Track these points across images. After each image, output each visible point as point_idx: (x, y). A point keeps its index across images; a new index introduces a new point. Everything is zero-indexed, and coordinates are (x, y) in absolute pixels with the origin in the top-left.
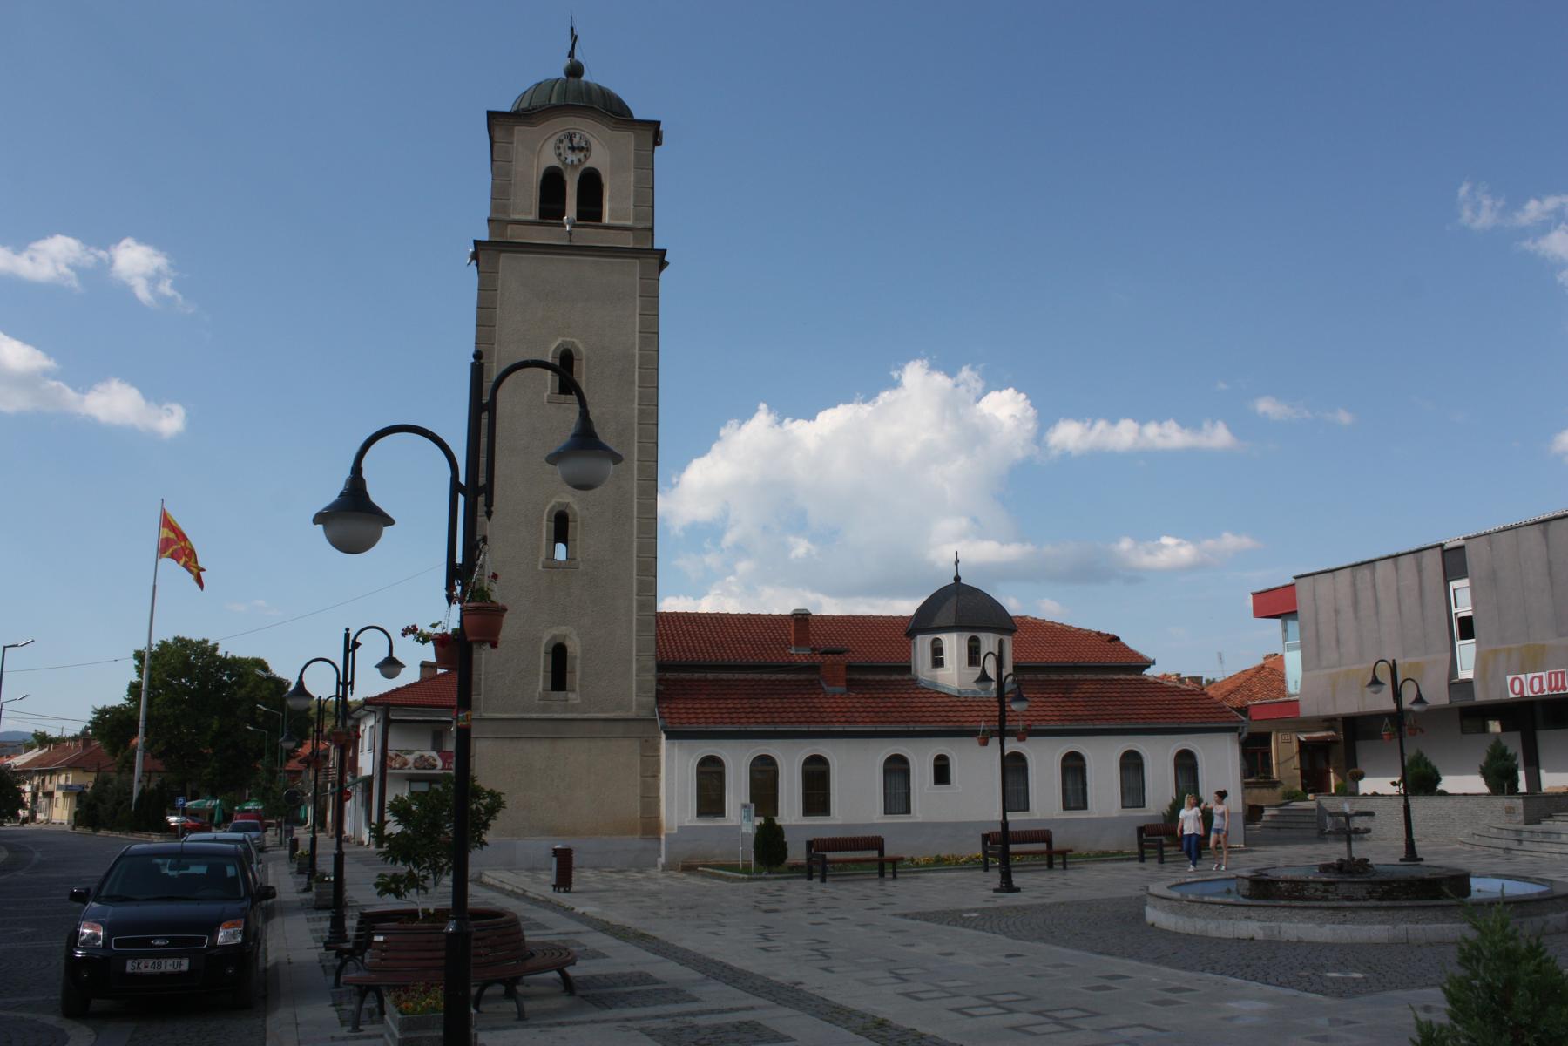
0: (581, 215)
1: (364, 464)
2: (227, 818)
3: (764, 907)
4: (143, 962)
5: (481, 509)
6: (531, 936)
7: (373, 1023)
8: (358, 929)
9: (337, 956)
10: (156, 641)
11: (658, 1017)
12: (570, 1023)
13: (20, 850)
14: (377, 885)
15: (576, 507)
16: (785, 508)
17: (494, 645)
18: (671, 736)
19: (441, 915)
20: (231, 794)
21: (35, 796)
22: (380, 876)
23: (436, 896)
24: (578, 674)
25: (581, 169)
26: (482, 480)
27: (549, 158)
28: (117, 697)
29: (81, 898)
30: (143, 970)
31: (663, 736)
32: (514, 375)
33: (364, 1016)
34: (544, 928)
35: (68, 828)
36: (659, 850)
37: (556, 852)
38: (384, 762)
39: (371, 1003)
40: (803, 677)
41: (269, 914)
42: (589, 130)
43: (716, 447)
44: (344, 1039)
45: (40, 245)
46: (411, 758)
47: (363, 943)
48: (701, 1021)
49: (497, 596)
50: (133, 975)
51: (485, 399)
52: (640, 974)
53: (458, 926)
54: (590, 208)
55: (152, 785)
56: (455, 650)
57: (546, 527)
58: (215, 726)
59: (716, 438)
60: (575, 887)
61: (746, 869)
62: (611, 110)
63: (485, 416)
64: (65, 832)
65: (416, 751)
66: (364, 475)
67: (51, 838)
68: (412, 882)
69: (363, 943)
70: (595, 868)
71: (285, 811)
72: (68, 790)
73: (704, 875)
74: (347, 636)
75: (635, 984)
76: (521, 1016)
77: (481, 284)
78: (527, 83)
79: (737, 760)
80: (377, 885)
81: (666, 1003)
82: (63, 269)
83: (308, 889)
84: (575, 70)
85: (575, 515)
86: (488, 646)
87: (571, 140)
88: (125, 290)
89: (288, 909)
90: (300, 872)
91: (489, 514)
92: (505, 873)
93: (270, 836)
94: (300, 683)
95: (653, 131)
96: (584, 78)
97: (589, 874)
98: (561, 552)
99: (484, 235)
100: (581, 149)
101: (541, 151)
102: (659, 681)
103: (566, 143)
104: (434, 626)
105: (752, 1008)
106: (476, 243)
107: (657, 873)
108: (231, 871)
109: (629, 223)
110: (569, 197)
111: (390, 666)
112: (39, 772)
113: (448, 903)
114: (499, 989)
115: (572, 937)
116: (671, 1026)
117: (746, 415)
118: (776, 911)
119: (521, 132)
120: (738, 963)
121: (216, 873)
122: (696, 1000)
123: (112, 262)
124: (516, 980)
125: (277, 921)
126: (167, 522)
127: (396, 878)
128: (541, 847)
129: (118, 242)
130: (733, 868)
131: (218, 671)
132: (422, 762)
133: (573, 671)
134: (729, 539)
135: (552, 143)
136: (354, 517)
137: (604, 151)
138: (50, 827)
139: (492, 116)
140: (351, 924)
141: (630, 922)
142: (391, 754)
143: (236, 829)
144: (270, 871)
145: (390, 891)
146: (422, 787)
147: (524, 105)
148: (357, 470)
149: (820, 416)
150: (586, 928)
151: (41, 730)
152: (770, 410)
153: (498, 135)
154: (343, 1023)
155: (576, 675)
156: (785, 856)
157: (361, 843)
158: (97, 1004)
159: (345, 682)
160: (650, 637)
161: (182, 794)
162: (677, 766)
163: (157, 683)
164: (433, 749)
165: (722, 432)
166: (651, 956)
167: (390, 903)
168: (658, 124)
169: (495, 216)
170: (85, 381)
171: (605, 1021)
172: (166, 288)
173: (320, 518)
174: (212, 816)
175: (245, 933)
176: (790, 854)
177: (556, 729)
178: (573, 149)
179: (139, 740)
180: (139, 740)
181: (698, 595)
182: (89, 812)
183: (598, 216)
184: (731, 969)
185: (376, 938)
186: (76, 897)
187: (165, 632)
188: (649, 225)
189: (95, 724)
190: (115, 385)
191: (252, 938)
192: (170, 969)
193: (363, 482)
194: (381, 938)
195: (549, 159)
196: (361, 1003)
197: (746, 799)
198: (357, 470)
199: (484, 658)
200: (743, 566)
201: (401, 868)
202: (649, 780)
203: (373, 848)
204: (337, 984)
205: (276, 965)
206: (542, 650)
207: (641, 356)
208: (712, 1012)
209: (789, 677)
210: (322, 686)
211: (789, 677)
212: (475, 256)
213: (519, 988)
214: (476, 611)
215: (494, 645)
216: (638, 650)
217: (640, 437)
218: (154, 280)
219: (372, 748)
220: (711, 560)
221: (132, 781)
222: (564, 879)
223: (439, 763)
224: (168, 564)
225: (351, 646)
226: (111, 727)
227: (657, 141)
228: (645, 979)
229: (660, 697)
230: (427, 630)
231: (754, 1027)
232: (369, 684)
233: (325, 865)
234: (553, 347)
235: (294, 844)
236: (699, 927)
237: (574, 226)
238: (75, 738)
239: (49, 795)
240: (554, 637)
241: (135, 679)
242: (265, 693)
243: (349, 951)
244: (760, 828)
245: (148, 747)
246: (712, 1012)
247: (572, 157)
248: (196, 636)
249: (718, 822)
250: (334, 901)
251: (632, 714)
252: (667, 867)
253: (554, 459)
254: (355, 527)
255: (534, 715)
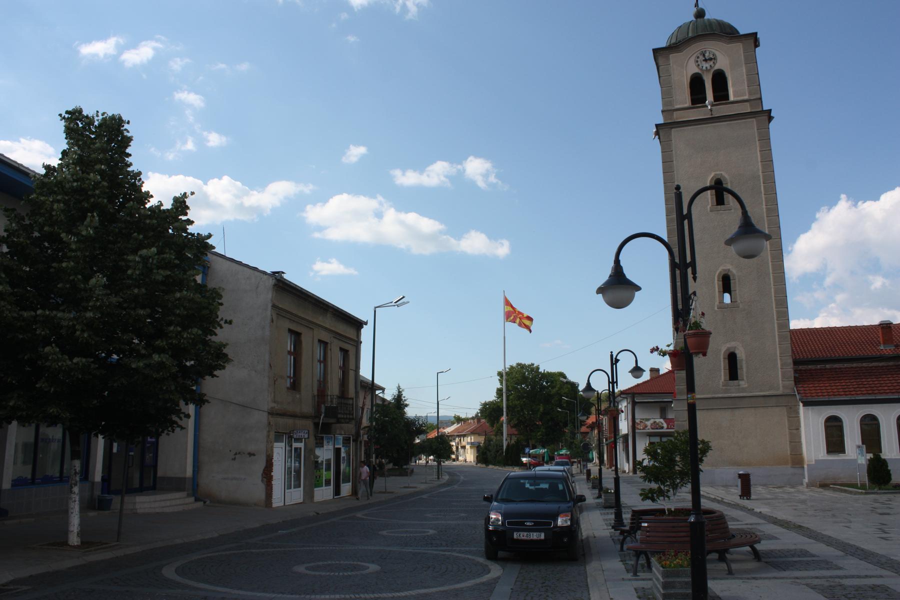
0: (716, 98)
1: (620, 258)
3: (879, 511)
4: (522, 533)
5: (690, 276)
6: (732, 525)
7: (644, 572)
8: (632, 519)
9: (621, 534)
10: (508, 366)
11: (817, 578)
12: (761, 578)
13: (454, 473)
15: (734, 271)
16: (865, 259)
17: (705, 354)
18: (806, 404)
19: (685, 512)
20: (552, 446)
21: (457, 448)
22: (642, 490)
24: (745, 370)
26: (689, 260)
27: (692, 69)
28: (492, 397)
29: (489, 499)
31: (801, 404)
32: (701, 195)
33: (639, 568)
35: (474, 464)
36: (803, 475)
37: (740, 476)
38: (634, 426)
40: (891, 363)
41: (581, 511)
42: (712, 47)
43: (814, 226)
44: (630, 580)
45: (430, 168)
46: (649, 423)
47: (635, 526)
48: (847, 582)
50: (517, 540)
51: (685, 212)
52: (801, 550)
53: (696, 518)
54: (721, 92)
55: (513, 442)
56: (682, 357)
57: (717, 285)
59: (814, 219)
60: (753, 497)
61: (863, 486)
62: (725, 32)
63: (686, 222)
64: (473, 466)
65: (651, 419)
66: (622, 264)
67: (465, 469)
68: (661, 493)
69: (635, 526)
70: (764, 485)
71: (581, 454)
72: (472, 444)
73: (834, 490)
74: (612, 356)
75: (799, 556)
76: (730, 572)
77: (662, 149)
78: (673, 28)
79: (851, 419)
80: (641, 495)
82: (443, 178)
83: (599, 497)
84: (700, 14)
85: (734, 275)
86: (701, 355)
87: (704, 56)
88: (472, 184)
89: (590, 508)
90: (594, 487)
91: (695, 278)
92: (717, 489)
93: (575, 469)
94: (589, 384)
97: (760, 488)
98: (727, 298)
100: (711, 59)
101: (687, 65)
102: (795, 371)
103: (701, 58)
104: (668, 346)
105: (881, 576)
106: (657, 126)
107: (803, 488)
108: (561, 487)
109: (746, 97)
110: (709, 89)
111: (637, 371)
112: (459, 436)
113: (689, 505)
116: (827, 584)
117: (832, 203)
118: (888, 514)
119: (673, 57)
121: (553, 488)
122: (840, 568)
123: (464, 170)
124: (726, 551)
126: (507, 303)
127: (651, 491)
128: (731, 473)
129: (466, 159)
131: (540, 380)
132: (655, 425)
133: (742, 368)
134: (828, 281)
135: (692, 60)
136: (618, 288)
137: (725, 57)
139: (656, 52)
140: (627, 517)
141: (789, 518)
142: (637, 421)
143: (557, 464)
146: (656, 440)
147: (673, 41)
148: (617, 261)
149: (883, 197)
150: (762, 521)
151: (458, 414)
152: (848, 199)
153: (661, 62)
154: (628, 571)
155: (743, 369)
156: (890, 479)
157: (624, 472)
158: (501, 554)
159: (613, 382)
160: (787, 345)
161: (528, 446)
162: (811, 424)
163: (510, 388)
165: (818, 216)
167: (648, 505)
168: (756, 34)
170: (459, 237)
172: (492, 179)
173: (600, 290)
174: (543, 458)
175: (571, 520)
176: (893, 477)
177: (733, 403)
178: (706, 60)
179: (504, 418)
180: (504, 418)
181: (812, 317)
182: (484, 455)
183: (726, 97)
184: (862, 550)
187: (512, 362)
188: (758, 96)
189: (482, 411)
190: (473, 233)
191: (575, 522)
192: (535, 538)
193: (621, 268)
194: (646, 525)
195: (693, 69)
196: (638, 560)
198: (617, 261)
200: (840, 297)
201: (654, 486)
202: (795, 431)
203: (631, 474)
205: (588, 538)
206: (722, 357)
207: (764, 176)
208: (853, 577)
209: (881, 364)
210: (601, 385)
211: (881, 364)
212: (657, 133)
213: (728, 556)
215: (705, 354)
218: (486, 176)
219: (627, 418)
220: (819, 295)
221: (502, 440)
222: (746, 492)
223: (665, 425)
224: (509, 325)
225: (614, 362)
226: (490, 412)
227: (756, 44)
228: (805, 553)
229: (797, 381)
230: (665, 348)
231: (885, 589)
232: (626, 382)
233: (608, 483)
235: (589, 472)
237: (712, 105)
238: (473, 418)
239: (464, 447)
240: (728, 349)
241: (499, 386)
242: (566, 390)
244: (870, 460)
246: (853, 577)
247: (706, 65)
248: (527, 362)
249: (841, 457)
250: (616, 504)
251: (780, 392)
252: (810, 485)
253: (729, 242)
254: (620, 294)
255: (720, 395)
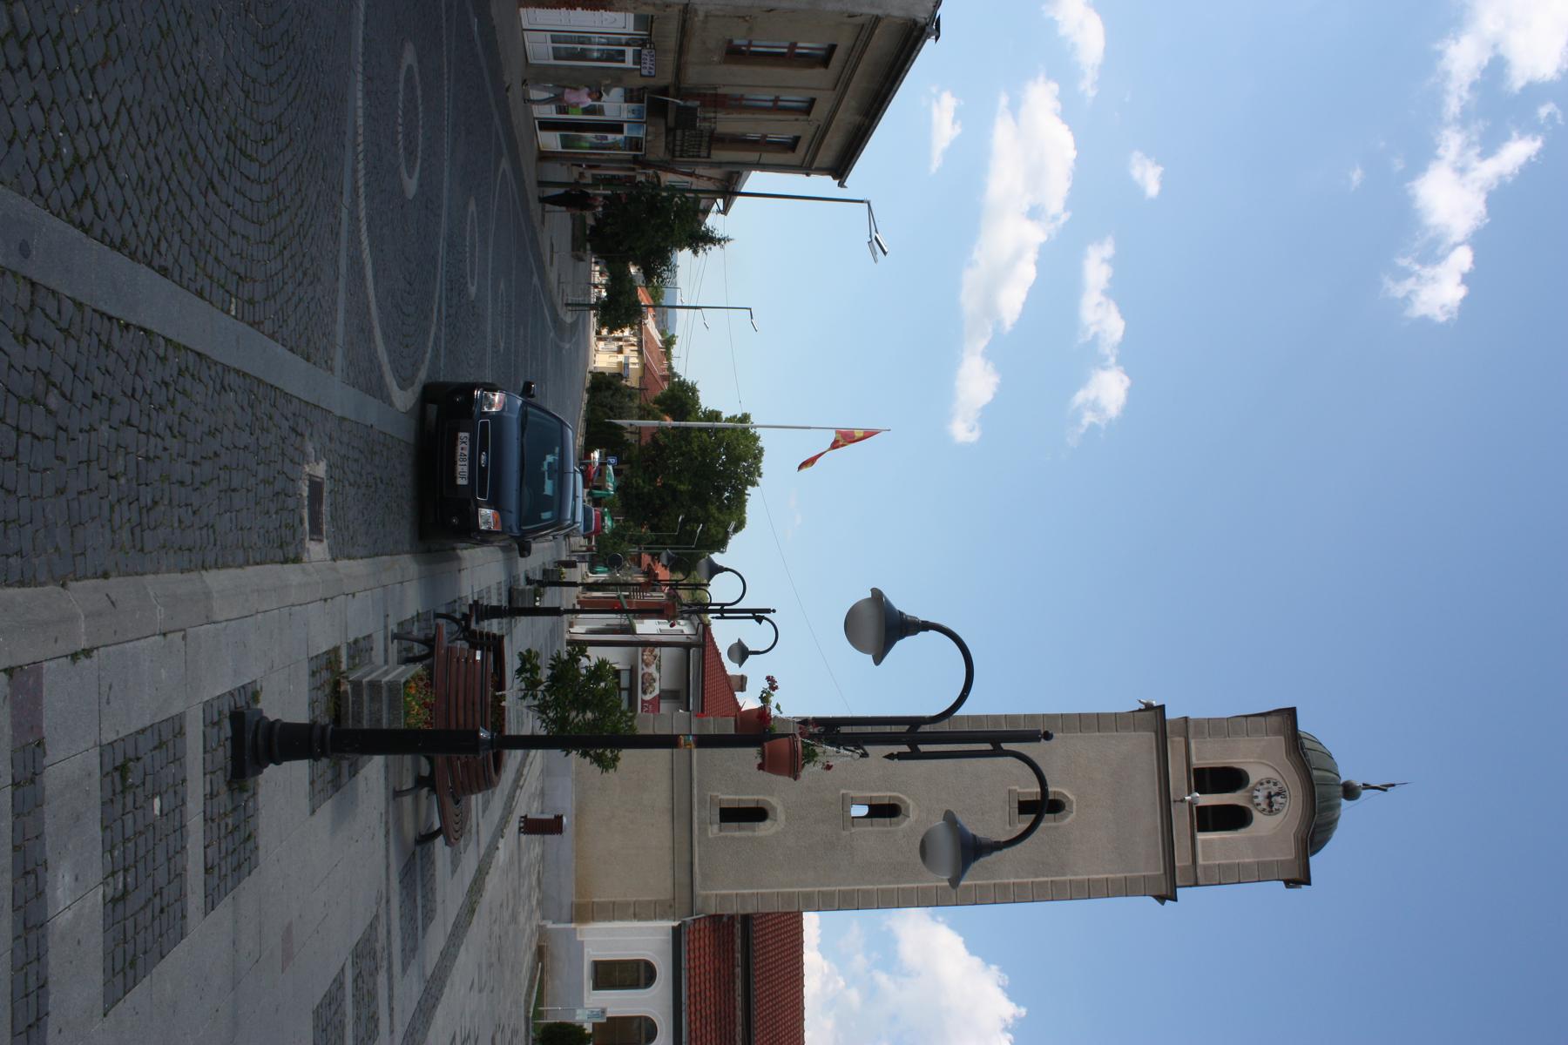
0: (1202, 811)
1: (933, 634)
2: (597, 502)
4: (467, 446)
5: (895, 749)
6: (476, 800)
7: (399, 652)
8: (488, 634)
10: (759, 432)
11: (389, 932)
12: (387, 843)
14: (529, 651)
17: (761, 767)
18: (676, 931)
20: (619, 504)
21: (619, 339)
23: (522, 718)
24: (737, 834)
25: (1250, 806)
28: (708, 400)
29: (527, 391)
30: (460, 446)
31: (676, 924)
33: (405, 644)
34: (484, 811)
35: (591, 368)
37: (559, 818)
39: (418, 649)
41: (505, 549)
44: (386, 627)
45: (1113, 309)
46: (652, 669)
48: (382, 978)
49: (810, 771)
50: (456, 438)
51: (1005, 746)
52: (433, 911)
53: (485, 741)
54: (1212, 819)
55: (627, 436)
56: (757, 730)
57: (883, 795)
58: (682, 487)
59: (988, 960)
60: (524, 837)
61: (539, 1014)
62: (1315, 833)
63: (988, 747)
64: (586, 364)
65: (660, 673)
66: (921, 634)
68: (532, 685)
70: (543, 857)
71: (604, 554)
73: (533, 970)
74: (768, 611)
76: (397, 794)
78: (1330, 745)
80: (529, 651)
81: (403, 939)
82: (1093, 330)
83: (529, 581)
84: (1350, 792)
85: (898, 824)
86: (759, 761)
87: (1278, 794)
88: (1083, 381)
90: (545, 572)
91: (890, 757)
92: (538, 778)
93: (579, 542)
94: (722, 570)
95: (1300, 878)
96: (1344, 801)
98: (860, 811)
99: (1170, 715)
100: (1270, 805)
101: (1263, 764)
102: (732, 918)
103: (1274, 790)
104: (778, 707)
105: (392, 1032)
106: (1162, 708)
108: (546, 515)
109: (1200, 861)
110: (1219, 796)
111: (741, 653)
112: (640, 342)
113: (511, 729)
114: (425, 770)
115: (474, 837)
116: (379, 946)
117: (1012, 993)
119: (1279, 743)
120: (440, 1012)
121: (547, 503)
123: (1105, 368)
124: (433, 789)
125: (500, 555)
127: (535, 669)
128: (564, 804)
129: (1127, 373)
130: (540, 1000)
131: (733, 487)
132: (649, 681)
133: (740, 829)
134: (882, 978)
136: (881, 626)
137: (1272, 829)
138: (592, 352)
139: (1291, 713)
140: (493, 626)
142: (657, 651)
143: (586, 512)
144: (546, 544)
145: (523, 664)
146: (625, 682)
147: (1307, 744)
148: (927, 626)
150: (482, 852)
153: (1274, 720)
154: (401, 624)
155: (737, 832)
157: (571, 625)
158: (432, 410)
159: (723, 611)
160: (776, 907)
161: (620, 462)
162: (646, 939)
164: (662, 691)
165: (994, 968)
166: (451, 920)
167: (512, 663)
169: (1191, 724)
171: (388, 879)
172: (1088, 418)
173: (877, 595)
174: (599, 488)
175: (489, 532)
177: (682, 815)
178: (1269, 796)
179: (669, 422)
180: (669, 422)
181: (821, 948)
182: (605, 385)
183: (1203, 828)
184: (434, 1006)
185: (478, 653)
186: (528, 386)
187: (766, 440)
188: (1201, 881)
189: (682, 384)
191: (485, 538)
192: (459, 469)
193: (915, 633)
195: (1256, 774)
197: (613, 1012)
198: (927, 626)
199: (750, 756)
200: (854, 996)
201: (544, 674)
203: (567, 636)
204: (438, 616)
205: (458, 558)
207: (1064, 883)
208: (391, 988)
210: (720, 590)
212: (1149, 707)
213: (425, 791)
214: (794, 751)
215: (761, 767)
216: (762, 895)
217: (981, 886)
218: (1095, 406)
220: (859, 961)
221: (631, 417)
222: (531, 826)
223: (648, 697)
225: (758, 615)
226: (680, 398)
227: (1291, 883)
228: (429, 916)
229: (715, 919)
230: (774, 701)
232: (724, 633)
233: (551, 597)
234: (1066, 792)
236: (479, 966)
237: (1191, 804)
238: (670, 368)
239: (620, 351)
240: (774, 809)
241: (724, 416)
243: (467, 627)
244: (581, 1029)
245: (663, 430)
246: (391, 988)
247: (1261, 796)
249: (588, 983)
250: (514, 609)
251: (698, 890)
252: (542, 931)
253: (950, 818)
254: (870, 629)
255: (695, 791)
